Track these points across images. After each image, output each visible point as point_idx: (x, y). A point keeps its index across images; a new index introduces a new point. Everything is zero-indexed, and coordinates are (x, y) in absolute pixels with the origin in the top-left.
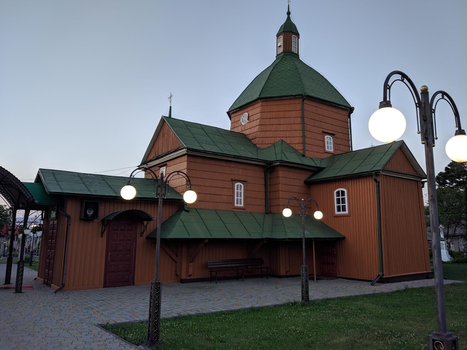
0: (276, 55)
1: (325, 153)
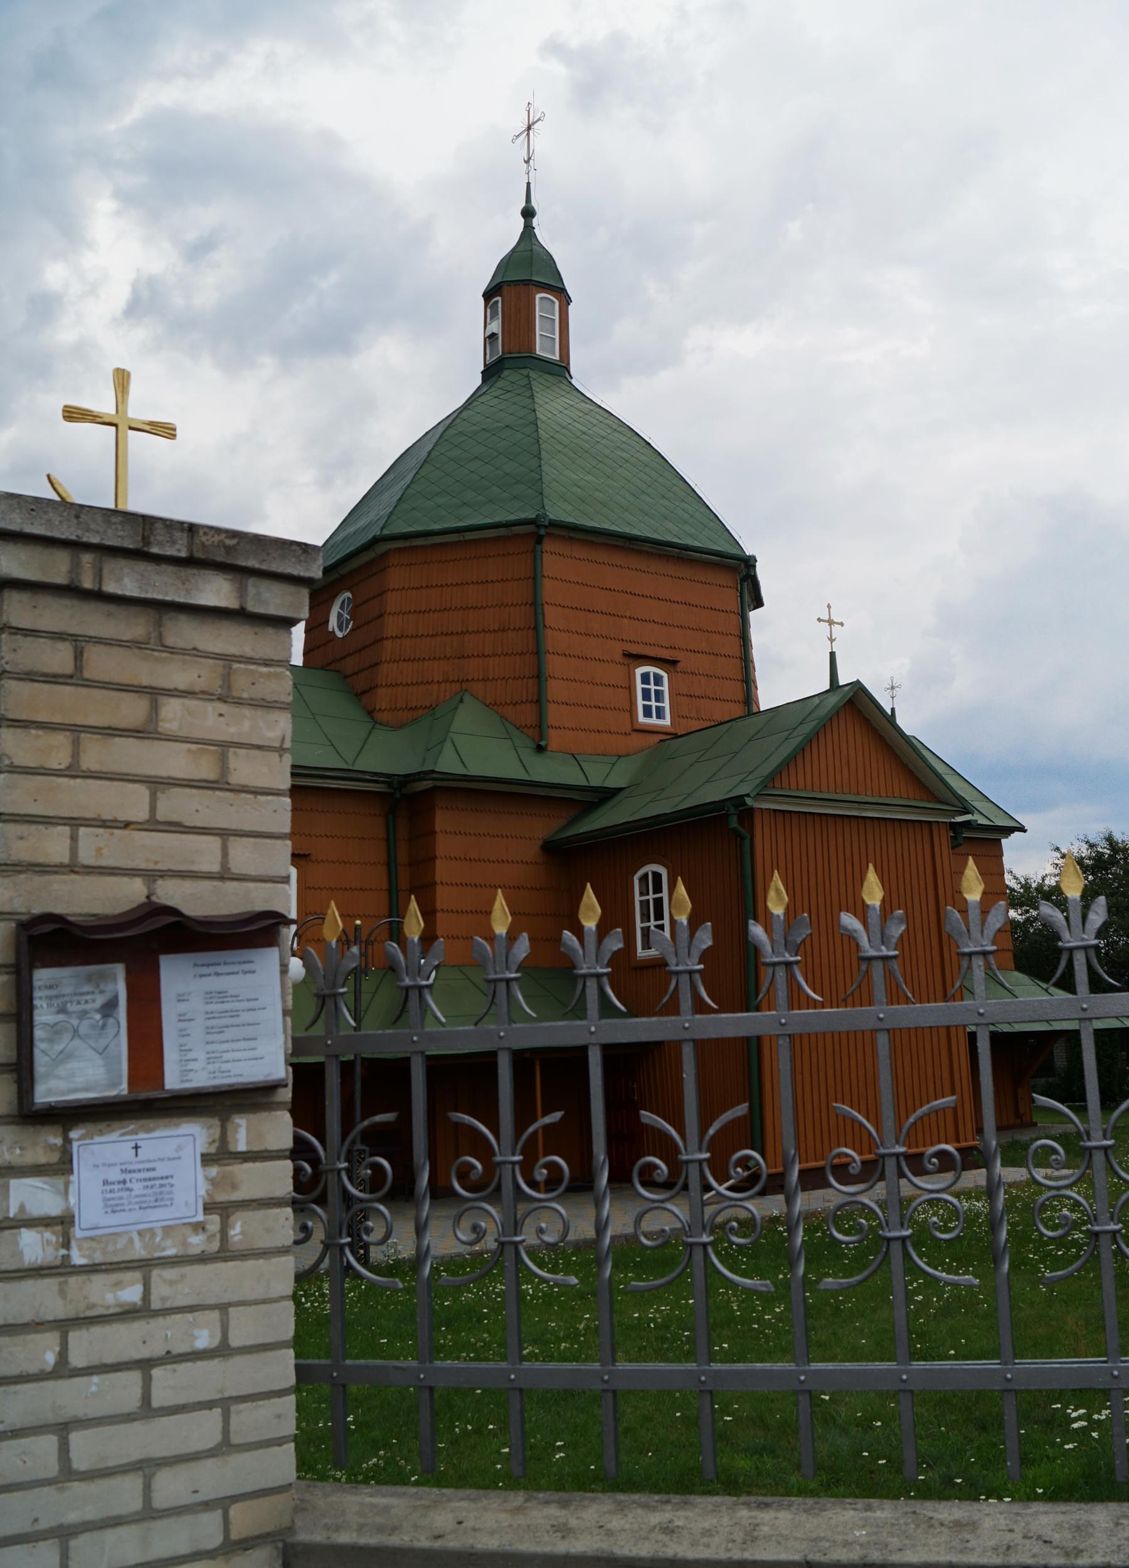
0: (482, 368)
1: (634, 733)
